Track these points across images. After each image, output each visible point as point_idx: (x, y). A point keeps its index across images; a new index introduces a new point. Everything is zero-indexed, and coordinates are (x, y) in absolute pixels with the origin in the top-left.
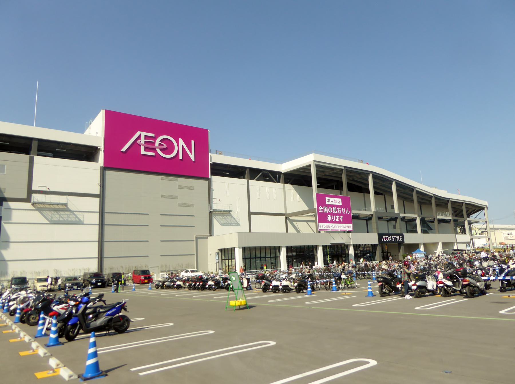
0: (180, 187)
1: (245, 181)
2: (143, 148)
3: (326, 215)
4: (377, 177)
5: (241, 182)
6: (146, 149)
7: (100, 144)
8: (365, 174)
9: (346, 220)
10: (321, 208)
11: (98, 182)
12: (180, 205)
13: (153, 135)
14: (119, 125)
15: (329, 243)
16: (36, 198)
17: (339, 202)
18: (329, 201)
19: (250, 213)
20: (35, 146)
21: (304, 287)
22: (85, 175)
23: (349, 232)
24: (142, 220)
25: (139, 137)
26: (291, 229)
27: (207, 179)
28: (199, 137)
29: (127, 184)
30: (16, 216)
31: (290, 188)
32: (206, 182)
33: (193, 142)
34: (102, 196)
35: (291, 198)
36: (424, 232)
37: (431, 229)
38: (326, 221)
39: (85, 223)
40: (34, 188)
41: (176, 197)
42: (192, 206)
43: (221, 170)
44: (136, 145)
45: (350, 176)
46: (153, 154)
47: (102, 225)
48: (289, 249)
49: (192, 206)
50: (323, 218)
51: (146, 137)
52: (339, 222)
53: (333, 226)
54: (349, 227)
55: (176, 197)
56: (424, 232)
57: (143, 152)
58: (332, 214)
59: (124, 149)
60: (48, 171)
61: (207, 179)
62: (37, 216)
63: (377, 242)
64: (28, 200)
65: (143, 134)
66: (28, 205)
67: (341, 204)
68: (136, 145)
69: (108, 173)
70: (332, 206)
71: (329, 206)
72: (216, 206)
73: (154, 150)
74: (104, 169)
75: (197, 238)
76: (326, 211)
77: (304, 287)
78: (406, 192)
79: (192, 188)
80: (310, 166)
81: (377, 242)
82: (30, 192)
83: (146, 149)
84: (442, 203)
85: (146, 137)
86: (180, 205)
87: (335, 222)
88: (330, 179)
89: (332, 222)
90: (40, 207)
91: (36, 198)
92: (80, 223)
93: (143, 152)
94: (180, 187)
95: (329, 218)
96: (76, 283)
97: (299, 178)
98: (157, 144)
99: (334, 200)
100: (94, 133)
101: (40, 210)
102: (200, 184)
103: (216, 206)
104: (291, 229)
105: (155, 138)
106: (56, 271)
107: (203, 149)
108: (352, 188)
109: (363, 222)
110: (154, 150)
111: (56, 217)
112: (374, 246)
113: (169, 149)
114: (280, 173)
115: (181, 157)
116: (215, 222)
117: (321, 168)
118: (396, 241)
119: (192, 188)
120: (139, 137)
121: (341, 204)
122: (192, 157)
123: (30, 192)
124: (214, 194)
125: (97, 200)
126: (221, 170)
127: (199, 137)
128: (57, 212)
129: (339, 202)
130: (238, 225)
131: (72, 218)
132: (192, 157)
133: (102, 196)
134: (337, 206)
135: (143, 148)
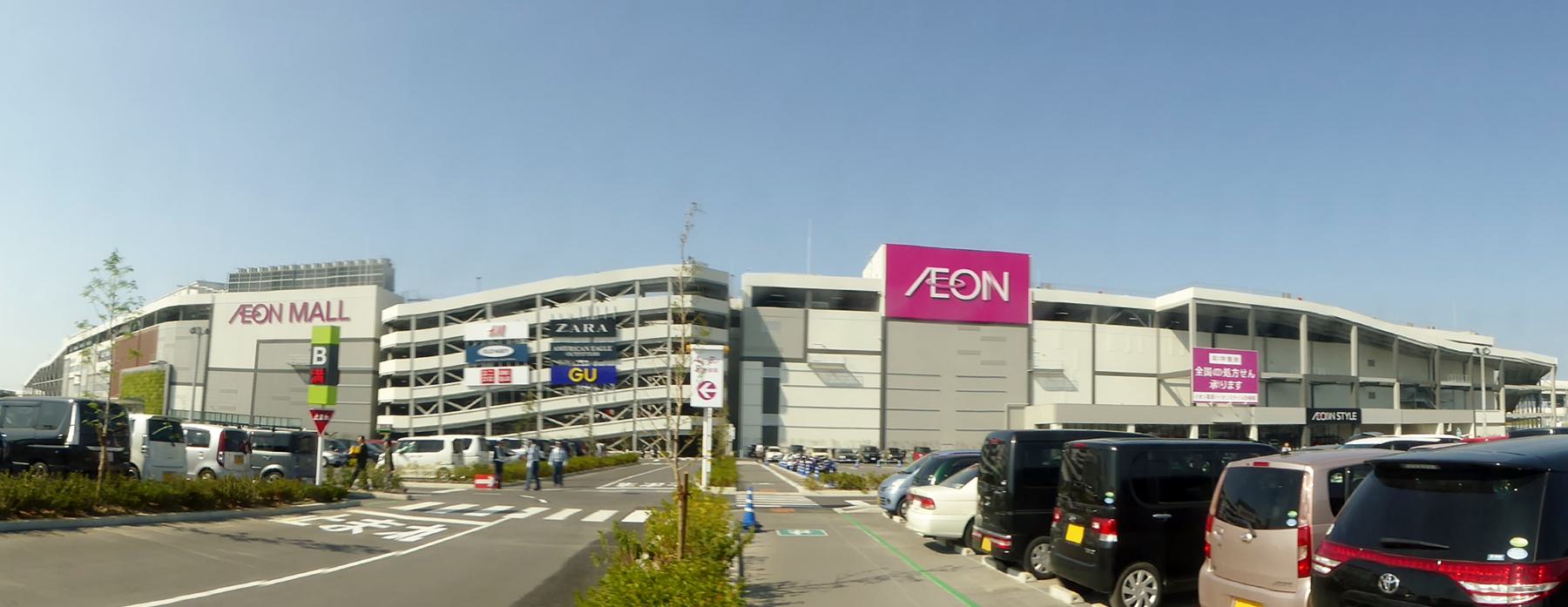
0: (984, 339)
1: (1089, 325)
2: (933, 289)
3: (1209, 379)
5: (1083, 328)
6: (939, 290)
8: (1296, 315)
9: (1248, 386)
10: (1199, 370)
11: (879, 336)
12: (983, 363)
13: (946, 270)
14: (903, 262)
15: (1210, 422)
17: (1237, 360)
18: (1214, 358)
19: (1095, 373)
20: (809, 296)
22: (863, 328)
23: (1252, 405)
25: (929, 276)
26: (1167, 400)
27: (1026, 325)
28: (1016, 267)
30: (793, 378)
31: (1167, 333)
32: (1025, 330)
33: (1006, 275)
34: (883, 353)
35: (1174, 351)
40: (810, 346)
41: (978, 353)
42: (1003, 363)
44: (924, 287)
46: (946, 296)
47: (884, 389)
49: (1003, 363)
50: (1202, 384)
51: (938, 274)
52: (1233, 391)
54: (1254, 397)
55: (978, 353)
57: (934, 294)
59: (909, 293)
60: (828, 327)
61: (1026, 325)
62: (813, 379)
63: (1304, 422)
64: (804, 360)
65: (934, 270)
66: (803, 366)
67: (1239, 363)
68: (924, 287)
69: (891, 324)
70: (1222, 367)
71: (1214, 366)
72: (1040, 362)
73: (948, 290)
74: (889, 317)
75: (1010, 408)
76: (1244, 372)
78: (1376, 341)
79: (1002, 339)
80: (1187, 306)
81: (1304, 422)
83: (939, 290)
85: (938, 274)
86: (983, 363)
87: (1227, 391)
88: (1221, 323)
90: (817, 369)
91: (812, 357)
92: (858, 386)
93: (934, 294)
94: (984, 339)
95: (1214, 385)
96: (850, 458)
97: (1174, 320)
98: (952, 283)
99: (1226, 359)
100: (874, 275)
101: (815, 371)
102: (1015, 334)
103: (1040, 362)
104: (1167, 400)
105: (948, 275)
106: (834, 442)
107: (1021, 282)
109: (1272, 390)
110: (948, 290)
111: (833, 379)
112: (1301, 427)
113: (968, 286)
114: (1152, 312)
115: (985, 297)
116: (1037, 387)
117: (1204, 309)
118: (1345, 421)
119: (1002, 339)
120: (929, 276)
121: (1239, 363)
122: (1005, 295)
123: (807, 351)
124: (1037, 347)
125: (879, 357)
127: (1016, 267)
128: (836, 376)
129: (1237, 360)
130: (1075, 389)
131: (850, 381)
132: (1005, 295)
133: (883, 353)
134: (1231, 367)
135: (933, 289)
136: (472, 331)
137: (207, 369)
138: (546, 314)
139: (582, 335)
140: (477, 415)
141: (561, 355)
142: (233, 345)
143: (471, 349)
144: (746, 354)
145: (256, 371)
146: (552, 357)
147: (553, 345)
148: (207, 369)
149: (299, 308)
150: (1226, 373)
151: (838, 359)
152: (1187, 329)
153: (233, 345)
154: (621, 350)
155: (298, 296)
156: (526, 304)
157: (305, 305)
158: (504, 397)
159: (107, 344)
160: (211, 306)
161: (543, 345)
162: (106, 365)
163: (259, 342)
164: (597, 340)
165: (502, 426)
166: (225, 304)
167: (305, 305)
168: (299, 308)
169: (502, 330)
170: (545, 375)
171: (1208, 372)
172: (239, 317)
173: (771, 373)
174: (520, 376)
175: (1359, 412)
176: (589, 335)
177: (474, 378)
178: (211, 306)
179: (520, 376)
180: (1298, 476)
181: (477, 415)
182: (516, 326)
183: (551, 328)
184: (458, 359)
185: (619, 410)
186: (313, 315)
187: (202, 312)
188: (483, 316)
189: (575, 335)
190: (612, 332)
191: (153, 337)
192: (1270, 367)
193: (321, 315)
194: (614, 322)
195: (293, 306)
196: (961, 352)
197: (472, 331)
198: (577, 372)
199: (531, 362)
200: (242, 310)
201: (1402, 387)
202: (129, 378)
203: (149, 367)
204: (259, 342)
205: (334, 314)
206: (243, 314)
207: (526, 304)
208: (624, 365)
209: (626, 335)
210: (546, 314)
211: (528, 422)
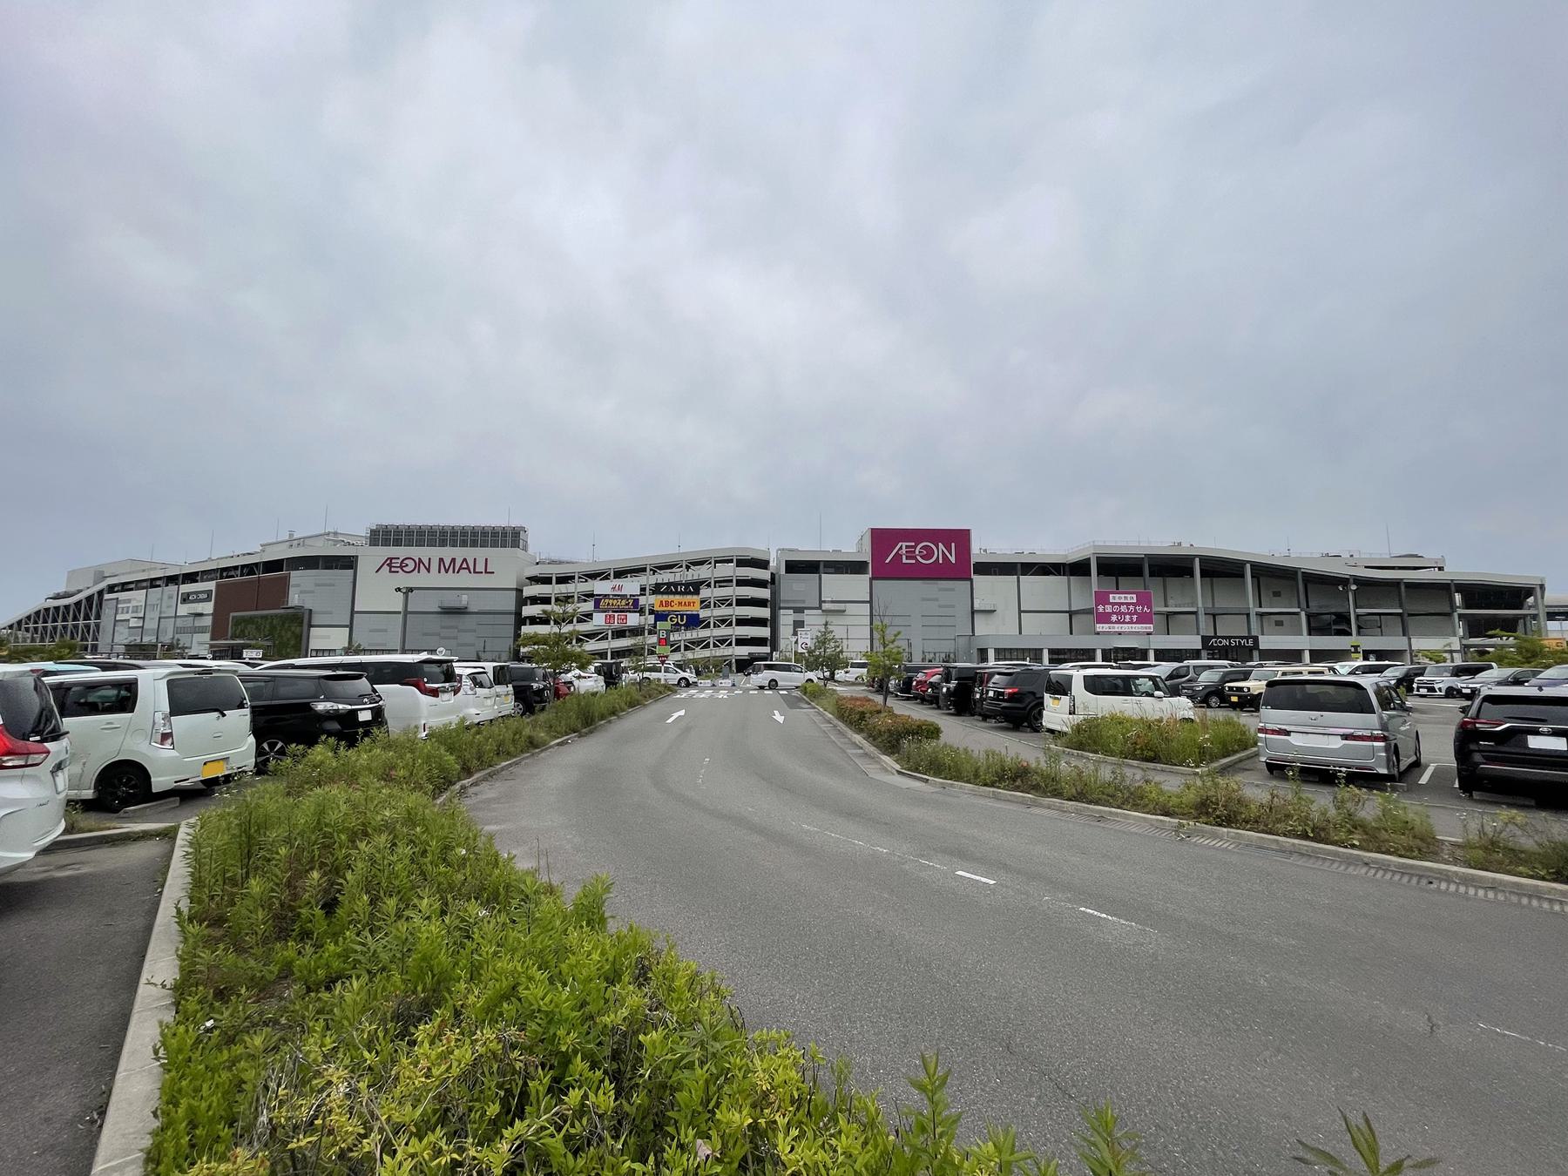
8: (1191, 558)
9: (1143, 618)
10: (1101, 608)
17: (1132, 598)
19: (1020, 612)
21: (274, 1129)
22: (857, 586)
28: (961, 538)
29: (890, 590)
32: (168, 846)
36: (1359, 633)
37: (1103, 1126)
38: (1109, 622)
43: (986, 569)
52: (1131, 622)
53: (1125, 628)
54: (1150, 627)
56: (1359, 633)
58: (1119, 613)
60: (835, 586)
70: (1120, 604)
71: (1114, 604)
74: (872, 579)
76: (1139, 608)
77: (274, 1129)
88: (1118, 568)
89: (1118, 622)
95: (1114, 618)
97: (1078, 569)
99: (1124, 598)
113: (929, 555)
123: (821, 602)
126: (986, 569)
127: (961, 538)
129: (1132, 598)
133: (870, 602)
136: (600, 587)
139: (676, 593)
140: (602, 645)
142: (378, 591)
143: (598, 600)
150: (1123, 609)
152: (1089, 574)
155: (448, 553)
157: (453, 560)
158: (619, 634)
159: (211, 585)
162: (208, 608)
165: (618, 654)
166: (371, 558)
167: (453, 560)
169: (620, 588)
171: (1109, 609)
173: (799, 617)
174: (633, 620)
175: (1256, 639)
176: (681, 593)
177: (599, 620)
179: (633, 620)
180: (1070, 677)
181: (602, 645)
183: (657, 589)
184: (589, 606)
185: (702, 643)
187: (348, 563)
188: (607, 578)
190: (697, 592)
191: (284, 584)
192: (1170, 602)
195: (441, 560)
197: (600, 587)
199: (642, 612)
200: (389, 562)
201: (1309, 616)
202: (237, 622)
205: (480, 567)
210: (665, 577)
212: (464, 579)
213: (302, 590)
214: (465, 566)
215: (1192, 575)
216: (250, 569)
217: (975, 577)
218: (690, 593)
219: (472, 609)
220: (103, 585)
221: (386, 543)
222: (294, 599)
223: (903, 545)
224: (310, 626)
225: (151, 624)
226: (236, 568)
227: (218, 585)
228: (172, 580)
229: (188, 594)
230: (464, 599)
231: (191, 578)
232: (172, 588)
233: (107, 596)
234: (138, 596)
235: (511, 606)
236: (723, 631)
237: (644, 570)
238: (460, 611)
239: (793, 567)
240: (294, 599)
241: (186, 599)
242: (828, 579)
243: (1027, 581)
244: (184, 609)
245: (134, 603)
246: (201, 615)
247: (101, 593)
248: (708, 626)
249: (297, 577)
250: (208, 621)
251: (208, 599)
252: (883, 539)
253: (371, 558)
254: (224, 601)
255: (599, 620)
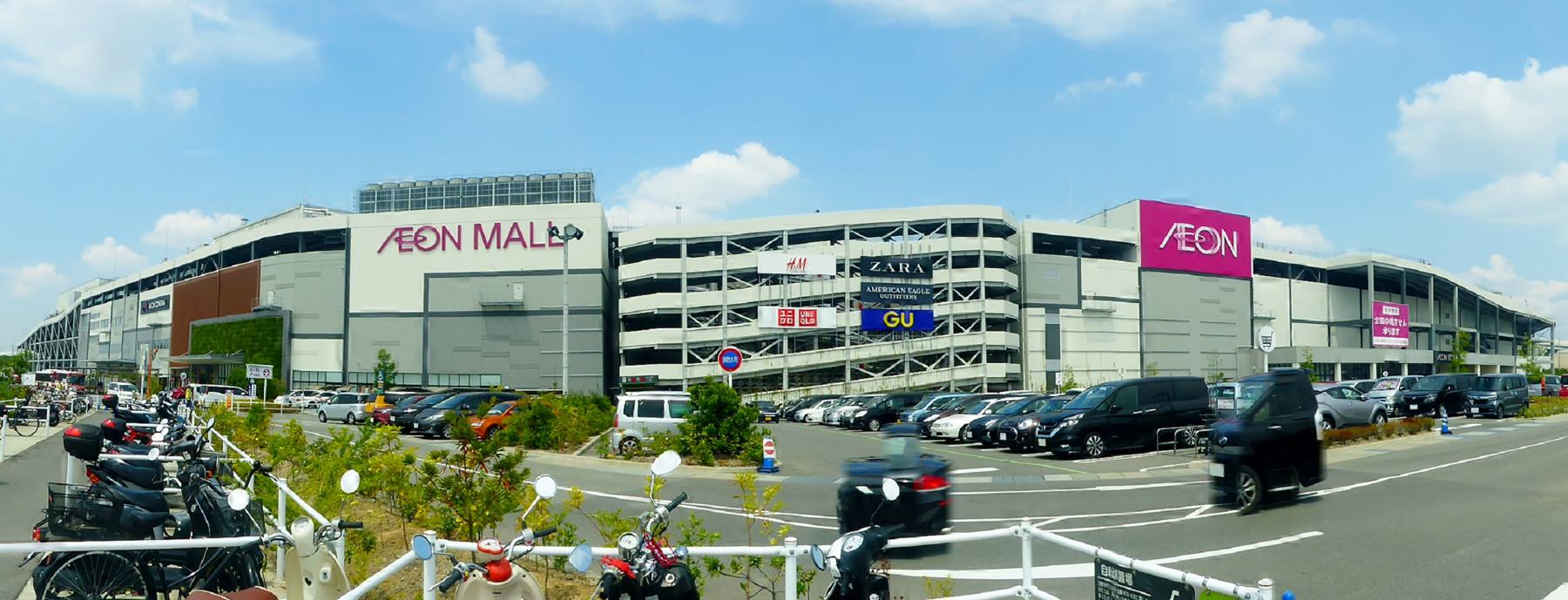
0: (1223, 289)
4: (1438, 280)
7: (1137, 242)
9: (1403, 333)
12: (1222, 311)
14: (1156, 216)
16: (1086, 304)
18: (1387, 310)
19: (1292, 321)
24: (1182, 328)
28: (1239, 225)
39: (1320, 288)
45: (101, 563)
48: (1344, 366)
49: (1233, 312)
55: (1217, 302)
56: (1482, 351)
58: (1389, 326)
60: (1099, 275)
64: (1079, 306)
66: (1077, 312)
68: (1173, 240)
74: (1140, 270)
82: (1081, 298)
83: (1188, 244)
84: (1507, 316)
85: (1187, 230)
86: (1222, 311)
93: (1185, 248)
94: (1223, 289)
95: (1385, 331)
100: (1128, 230)
103: (1257, 313)
105: (1193, 231)
108: (1411, 292)
113: (1209, 241)
122: (1235, 254)
123: (1081, 298)
127: (1239, 225)
132: (1235, 254)
137: (347, 315)
138: (874, 247)
139: (897, 274)
141: (875, 297)
142: (385, 280)
144: (1029, 301)
145: (426, 314)
146: (863, 295)
147: (863, 285)
148: (347, 315)
149: (488, 232)
151: (1105, 305)
153: (385, 280)
154: (939, 294)
155: (488, 215)
156: (834, 236)
157: (497, 227)
159: (168, 290)
160: (347, 231)
161: (854, 284)
162: (166, 317)
163: (427, 276)
164: (916, 282)
166: (368, 230)
167: (497, 227)
168: (488, 232)
169: (803, 263)
170: (854, 318)
172: (394, 246)
173: (1052, 320)
174: (828, 318)
176: (905, 275)
177: (769, 319)
178: (347, 231)
182: (821, 258)
183: (863, 266)
186: (510, 239)
187: (336, 240)
188: (774, 247)
189: (888, 274)
191: (255, 272)
193: (521, 239)
194: (927, 264)
195: (478, 227)
196: (1203, 301)
197: (766, 261)
198: (895, 318)
200: (398, 235)
202: (200, 331)
203: (250, 316)
204: (427, 276)
206: (399, 240)
207: (834, 236)
208: (938, 310)
209: (941, 276)
210: (874, 247)
211: (833, 373)
212: (516, 258)
213: (279, 285)
214: (515, 236)
215: (1426, 296)
216: (208, 263)
217: (1255, 277)
218: (917, 275)
219: (529, 307)
220: (80, 301)
221: (383, 206)
222: (268, 297)
223: (1180, 228)
224: (292, 336)
225: (116, 340)
226: (193, 265)
227: (176, 290)
228: (133, 288)
229: (148, 302)
230: (517, 293)
231: (148, 284)
232: (133, 297)
233: (83, 312)
234: (104, 309)
235: (596, 300)
236: (966, 339)
237: (691, 282)
238: (513, 311)
239: (1046, 244)
240: (268, 297)
241: (146, 308)
242: (1091, 266)
243: (1300, 286)
244: (144, 321)
245: (102, 317)
246: (160, 326)
247: (78, 308)
248: (943, 331)
249: (270, 265)
250: (166, 334)
251: (166, 307)
252: (1156, 216)
253: (368, 230)
254: (185, 306)
255: (769, 319)
